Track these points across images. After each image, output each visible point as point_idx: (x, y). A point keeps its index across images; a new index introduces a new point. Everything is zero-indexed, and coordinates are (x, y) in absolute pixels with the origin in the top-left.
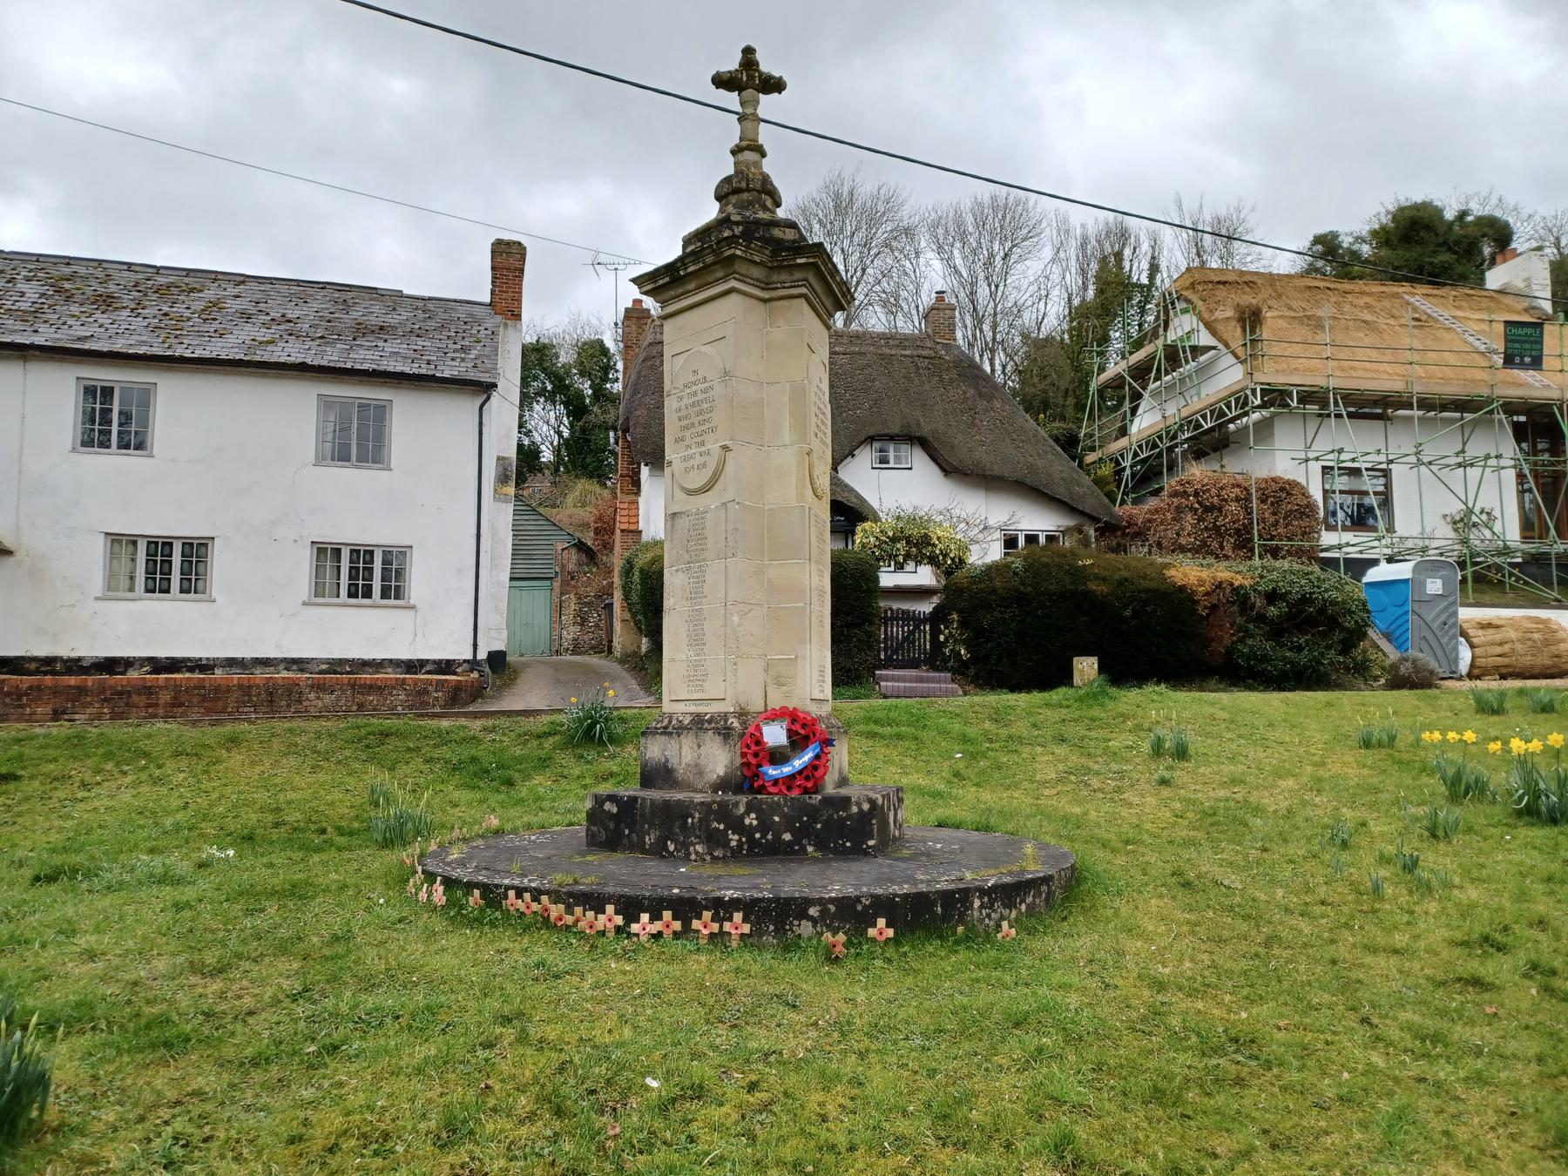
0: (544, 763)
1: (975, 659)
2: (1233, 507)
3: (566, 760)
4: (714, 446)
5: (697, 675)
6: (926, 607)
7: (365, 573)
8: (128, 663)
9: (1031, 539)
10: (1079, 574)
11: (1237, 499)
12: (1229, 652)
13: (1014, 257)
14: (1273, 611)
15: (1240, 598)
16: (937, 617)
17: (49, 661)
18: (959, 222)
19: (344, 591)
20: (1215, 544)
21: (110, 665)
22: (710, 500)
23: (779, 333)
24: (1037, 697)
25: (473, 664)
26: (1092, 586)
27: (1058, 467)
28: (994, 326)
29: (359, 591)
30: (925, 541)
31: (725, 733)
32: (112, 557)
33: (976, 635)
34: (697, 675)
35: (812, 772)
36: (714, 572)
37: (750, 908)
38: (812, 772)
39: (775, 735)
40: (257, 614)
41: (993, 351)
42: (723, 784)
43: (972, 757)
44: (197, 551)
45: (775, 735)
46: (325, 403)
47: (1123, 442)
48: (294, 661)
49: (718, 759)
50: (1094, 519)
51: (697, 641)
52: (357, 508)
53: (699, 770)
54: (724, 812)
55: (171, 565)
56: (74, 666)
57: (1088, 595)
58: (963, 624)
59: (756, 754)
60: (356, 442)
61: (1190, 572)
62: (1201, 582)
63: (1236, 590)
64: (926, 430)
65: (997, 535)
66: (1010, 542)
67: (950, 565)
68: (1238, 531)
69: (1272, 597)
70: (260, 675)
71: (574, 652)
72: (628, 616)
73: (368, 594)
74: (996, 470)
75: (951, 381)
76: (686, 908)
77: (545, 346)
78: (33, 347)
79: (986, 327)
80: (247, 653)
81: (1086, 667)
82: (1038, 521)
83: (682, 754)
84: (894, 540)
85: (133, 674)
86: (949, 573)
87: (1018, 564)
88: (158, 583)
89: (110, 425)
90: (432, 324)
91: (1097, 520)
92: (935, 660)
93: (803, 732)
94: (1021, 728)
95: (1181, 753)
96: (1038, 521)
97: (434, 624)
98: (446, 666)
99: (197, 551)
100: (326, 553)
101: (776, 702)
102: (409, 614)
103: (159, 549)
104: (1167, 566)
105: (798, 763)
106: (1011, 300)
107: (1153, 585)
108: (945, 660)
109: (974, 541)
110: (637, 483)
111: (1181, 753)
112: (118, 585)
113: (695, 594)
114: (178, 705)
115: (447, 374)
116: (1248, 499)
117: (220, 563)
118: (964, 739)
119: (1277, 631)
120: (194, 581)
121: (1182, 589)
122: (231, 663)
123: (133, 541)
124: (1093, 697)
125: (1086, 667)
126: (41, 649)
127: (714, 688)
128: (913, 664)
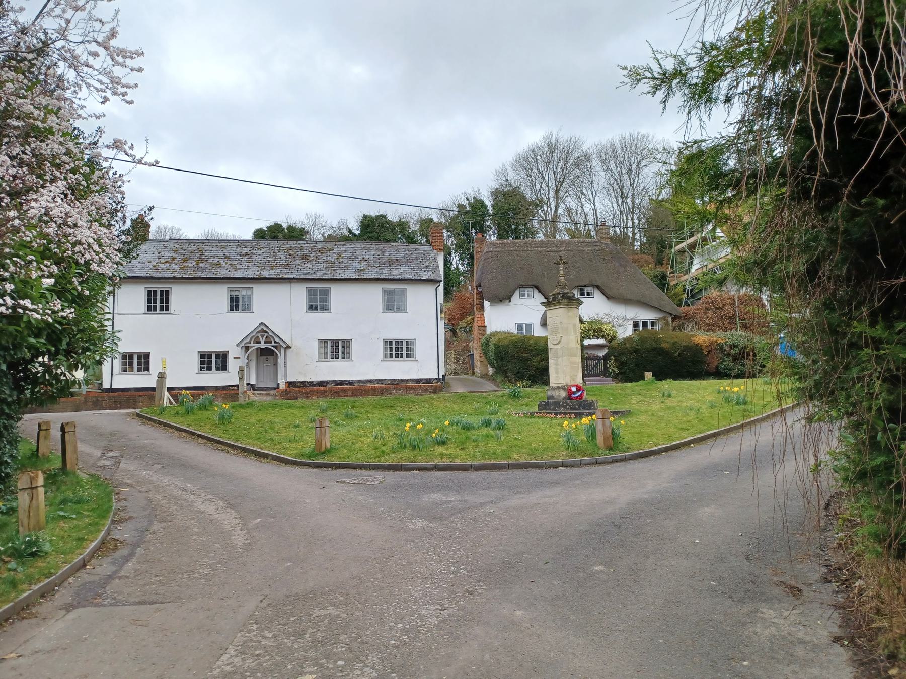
0: (506, 402)
1: (621, 373)
2: (728, 307)
3: (510, 401)
4: (559, 336)
5: (557, 379)
6: (601, 353)
7: (399, 349)
8: (327, 382)
9: (645, 324)
10: (658, 341)
11: (730, 304)
12: (717, 367)
13: (642, 165)
14: (733, 352)
15: (721, 347)
16: (606, 357)
17: (304, 383)
18: (614, 150)
19: (394, 355)
20: (721, 323)
21: (322, 383)
22: (558, 346)
23: (571, 314)
24: (634, 384)
25: (438, 380)
26: (663, 345)
27: (655, 293)
28: (633, 200)
29: (399, 355)
30: (600, 330)
31: (564, 389)
32: (320, 348)
33: (621, 365)
34: (557, 379)
35: (581, 396)
36: (560, 359)
37: (575, 414)
38: (581, 396)
39: (574, 389)
40: (367, 365)
41: (633, 213)
42: (565, 398)
43: (614, 399)
44: (346, 343)
45: (574, 389)
46: (385, 291)
47: (686, 277)
48: (380, 380)
49: (563, 394)
50: (671, 315)
51: (557, 373)
52: (397, 327)
53: (559, 396)
54: (566, 403)
55: (337, 349)
56: (311, 384)
57: (662, 349)
58: (616, 360)
59: (570, 393)
60: (393, 304)
61: (701, 338)
62: (705, 342)
63: (718, 344)
64: (598, 283)
65: (631, 322)
66: (636, 325)
67: (611, 339)
68: (730, 317)
69: (733, 346)
70: (369, 385)
71: (454, 374)
72: (483, 359)
73: (402, 357)
74: (629, 297)
75: (609, 260)
76: (565, 414)
77: (404, 223)
78: (294, 278)
79: (629, 201)
80: (365, 378)
81: (648, 375)
82: (647, 316)
83: (556, 393)
84: (589, 330)
85: (329, 386)
86: (610, 341)
87: (636, 338)
88: (335, 356)
89: (318, 304)
90: (413, 257)
91: (671, 315)
92: (606, 373)
93: (579, 389)
94: (628, 392)
95: (669, 396)
96: (647, 316)
97: (427, 364)
98: (429, 381)
99: (346, 343)
100: (388, 343)
101: (573, 383)
102: (416, 363)
103: (335, 343)
104: (693, 336)
105: (578, 394)
106: (642, 186)
107: (686, 344)
108: (610, 374)
109: (620, 325)
110: (483, 307)
111: (669, 396)
112: (323, 357)
113: (556, 364)
114: (335, 394)
115: (424, 278)
116: (734, 304)
117: (354, 347)
118: (613, 395)
119: (735, 359)
120: (346, 355)
121: (697, 345)
122: (359, 381)
123: (326, 342)
124: (650, 383)
125: (648, 375)
126: (301, 379)
127: (561, 381)
128: (598, 375)
